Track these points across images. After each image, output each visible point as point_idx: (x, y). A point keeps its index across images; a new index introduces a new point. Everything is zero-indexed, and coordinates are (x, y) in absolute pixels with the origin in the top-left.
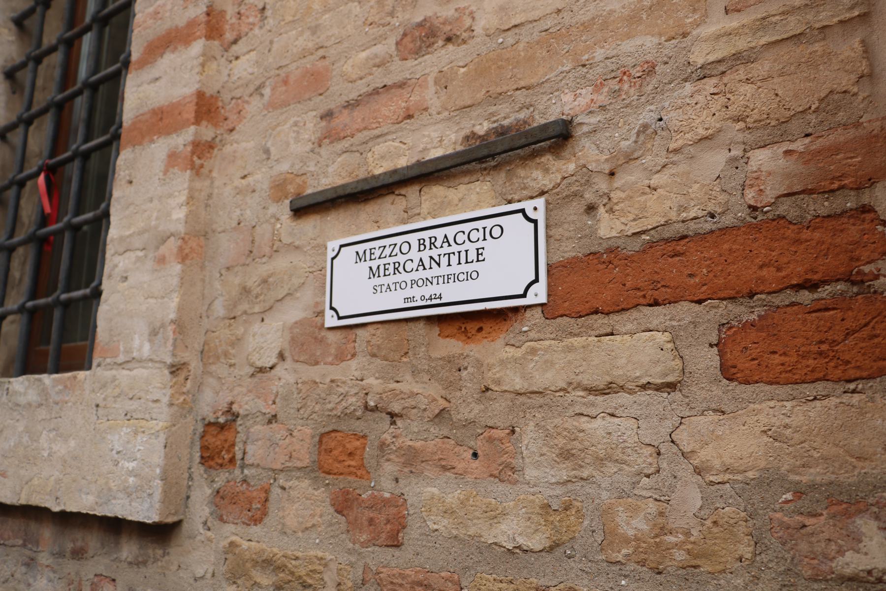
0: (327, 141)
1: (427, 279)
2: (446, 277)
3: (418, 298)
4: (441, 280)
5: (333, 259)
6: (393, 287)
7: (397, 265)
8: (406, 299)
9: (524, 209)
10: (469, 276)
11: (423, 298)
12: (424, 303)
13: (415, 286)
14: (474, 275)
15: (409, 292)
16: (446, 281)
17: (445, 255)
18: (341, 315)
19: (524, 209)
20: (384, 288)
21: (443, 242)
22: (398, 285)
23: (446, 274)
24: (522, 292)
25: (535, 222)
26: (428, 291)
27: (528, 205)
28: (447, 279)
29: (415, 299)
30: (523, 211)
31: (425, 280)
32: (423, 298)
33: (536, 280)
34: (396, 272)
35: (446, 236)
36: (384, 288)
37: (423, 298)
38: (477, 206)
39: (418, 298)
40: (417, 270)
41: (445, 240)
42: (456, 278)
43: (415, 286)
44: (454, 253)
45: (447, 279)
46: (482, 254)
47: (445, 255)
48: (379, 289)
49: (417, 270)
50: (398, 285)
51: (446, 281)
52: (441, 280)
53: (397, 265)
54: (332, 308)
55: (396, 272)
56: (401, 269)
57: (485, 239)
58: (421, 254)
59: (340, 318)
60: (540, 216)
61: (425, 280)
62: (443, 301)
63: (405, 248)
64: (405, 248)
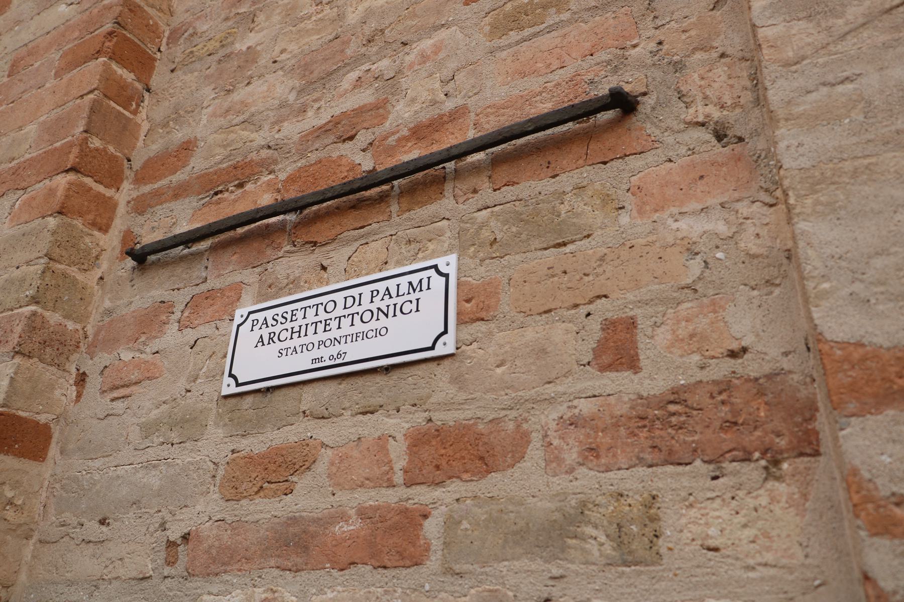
0: (445, 118)
1: (335, 339)
2: (355, 336)
3: (326, 358)
4: (349, 339)
5: (239, 326)
6: (299, 350)
7: (272, 335)
8: (314, 361)
9: (437, 265)
10: (378, 333)
11: (331, 358)
12: (332, 363)
13: (322, 347)
14: (383, 331)
15: (316, 354)
16: (354, 339)
17: (349, 315)
18: (240, 382)
19: (437, 265)
20: (290, 351)
21: (385, 295)
22: (305, 347)
23: (355, 333)
24: (430, 345)
25: (446, 276)
26: (334, 350)
27: (441, 262)
28: (356, 337)
29: (323, 360)
30: (435, 267)
31: (333, 340)
32: (331, 357)
33: (445, 332)
34: (271, 341)
35: (387, 289)
36: (290, 351)
37: (331, 358)
38: (372, 271)
39: (326, 358)
40: (292, 338)
41: (387, 293)
42: (365, 336)
43: (322, 347)
44: (321, 322)
45: (356, 337)
46: (329, 325)
47: (349, 315)
48: (284, 352)
49: (292, 338)
50: (305, 347)
51: (354, 339)
52: (349, 339)
53: (272, 335)
54: (231, 375)
55: (271, 341)
56: (275, 339)
57: (409, 293)
58: (261, 332)
59: (238, 385)
60: (452, 271)
61: (333, 340)
62: (346, 360)
63: (330, 307)
64: (330, 307)
